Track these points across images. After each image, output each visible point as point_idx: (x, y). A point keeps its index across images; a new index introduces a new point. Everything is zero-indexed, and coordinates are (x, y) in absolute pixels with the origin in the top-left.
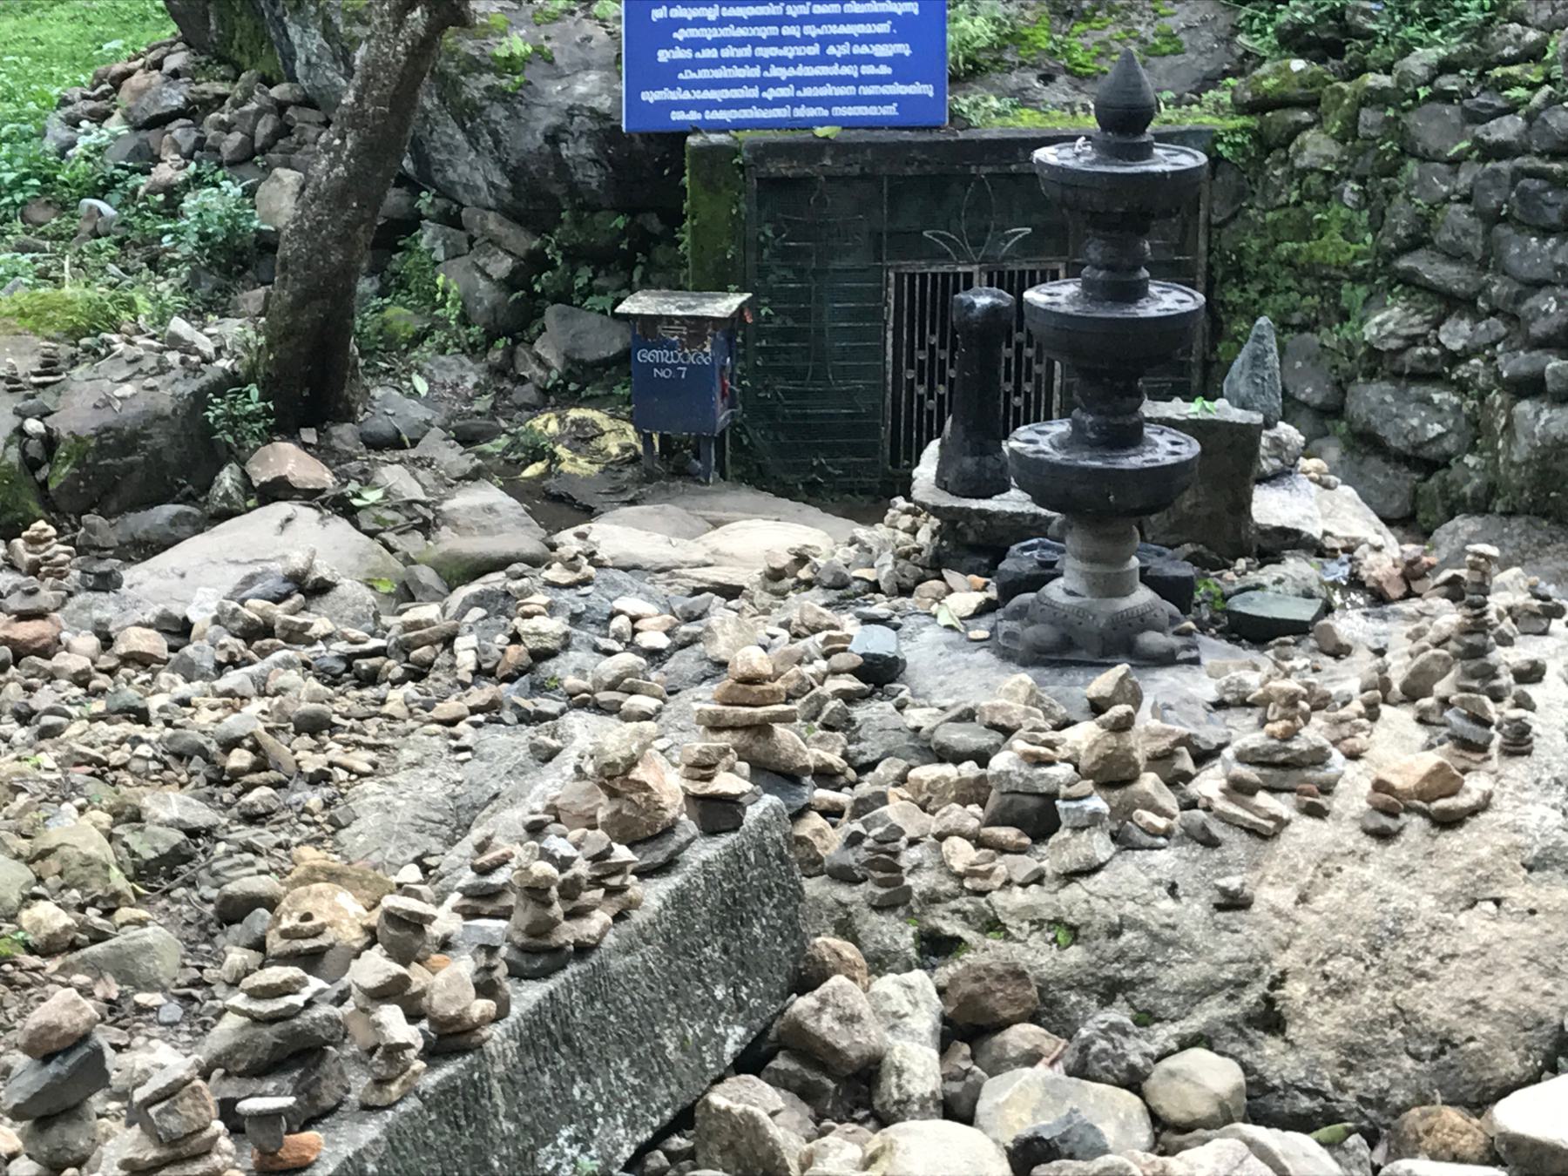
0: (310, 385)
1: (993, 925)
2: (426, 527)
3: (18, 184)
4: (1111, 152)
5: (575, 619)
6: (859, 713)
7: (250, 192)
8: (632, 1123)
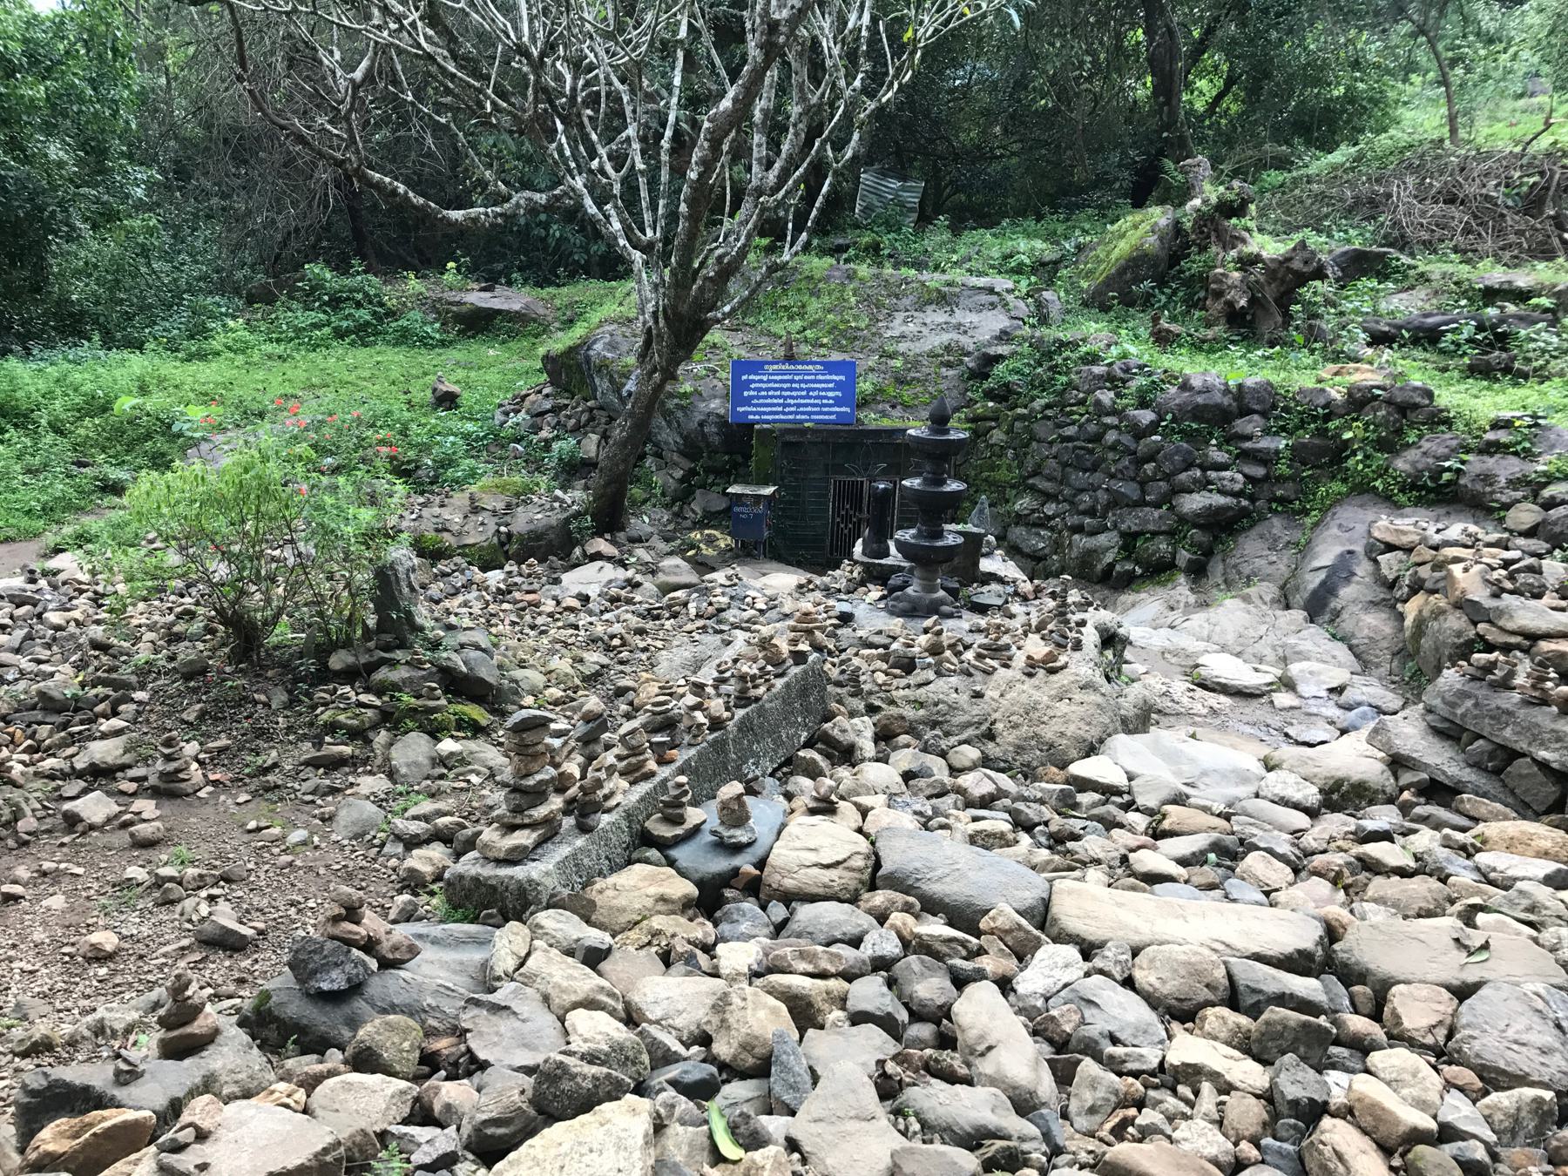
0: (609, 516)
1: (892, 702)
2: (653, 573)
3: (485, 437)
4: (933, 431)
5: (732, 598)
6: (839, 632)
7: (579, 442)
8: (771, 761)
